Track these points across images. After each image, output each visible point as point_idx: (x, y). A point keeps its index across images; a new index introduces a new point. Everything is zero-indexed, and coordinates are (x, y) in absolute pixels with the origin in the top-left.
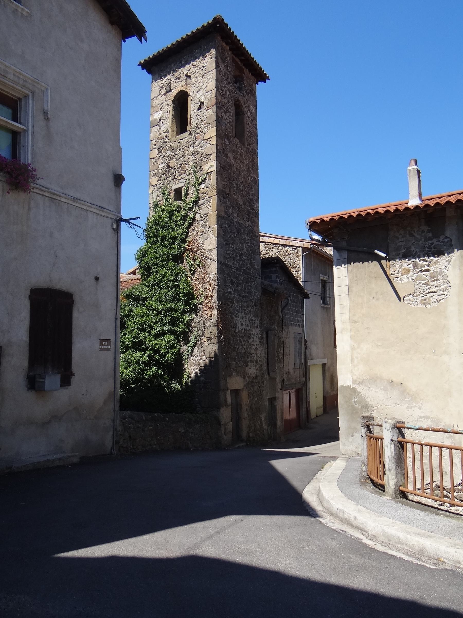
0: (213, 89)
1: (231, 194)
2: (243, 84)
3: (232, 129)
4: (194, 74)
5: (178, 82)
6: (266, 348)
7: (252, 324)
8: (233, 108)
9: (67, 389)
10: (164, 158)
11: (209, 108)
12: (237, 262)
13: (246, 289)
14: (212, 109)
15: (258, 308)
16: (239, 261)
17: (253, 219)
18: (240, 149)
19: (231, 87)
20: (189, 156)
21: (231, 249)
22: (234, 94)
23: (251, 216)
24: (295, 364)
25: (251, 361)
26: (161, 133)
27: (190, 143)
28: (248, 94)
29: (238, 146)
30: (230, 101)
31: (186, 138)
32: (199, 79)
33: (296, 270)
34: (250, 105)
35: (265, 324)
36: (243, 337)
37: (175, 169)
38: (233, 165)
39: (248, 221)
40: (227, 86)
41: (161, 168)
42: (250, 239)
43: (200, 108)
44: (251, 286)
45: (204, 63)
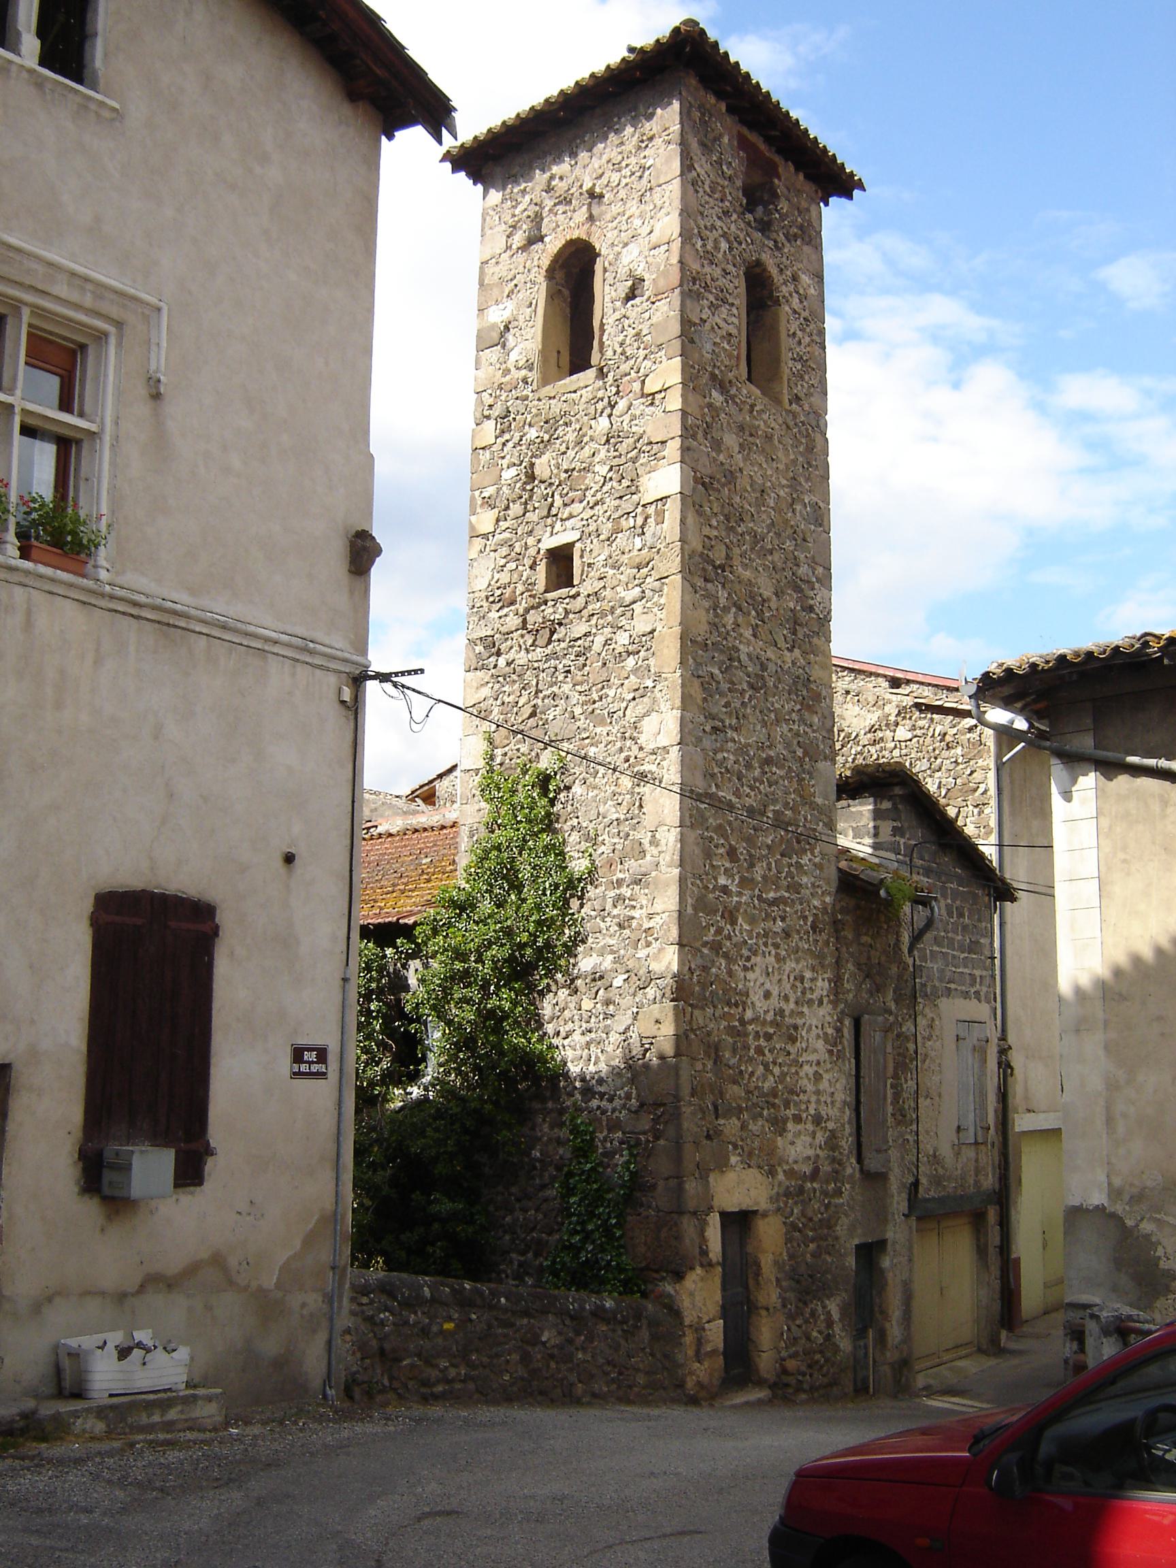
0: (673, 238)
1: (732, 566)
2: (777, 210)
3: (738, 358)
4: (615, 191)
5: (564, 213)
6: (854, 1073)
7: (803, 993)
8: (742, 290)
9: (192, 1193)
10: (519, 448)
11: (659, 297)
12: (752, 788)
13: (784, 875)
14: (668, 300)
15: (825, 937)
16: (757, 784)
17: (810, 642)
18: (765, 417)
19: (734, 226)
20: (596, 446)
21: (730, 744)
22: (744, 246)
23: (801, 632)
24: (959, 1127)
25: (798, 1119)
26: (509, 371)
27: (600, 406)
28: (791, 238)
29: (757, 408)
30: (730, 268)
31: (586, 387)
32: (628, 205)
33: (974, 799)
34: (800, 273)
35: (849, 991)
36: (768, 1037)
37: (551, 484)
38: (741, 470)
39: (790, 650)
40: (719, 223)
41: (509, 482)
42: (798, 707)
43: (631, 296)
44: (799, 866)
45: (645, 157)
